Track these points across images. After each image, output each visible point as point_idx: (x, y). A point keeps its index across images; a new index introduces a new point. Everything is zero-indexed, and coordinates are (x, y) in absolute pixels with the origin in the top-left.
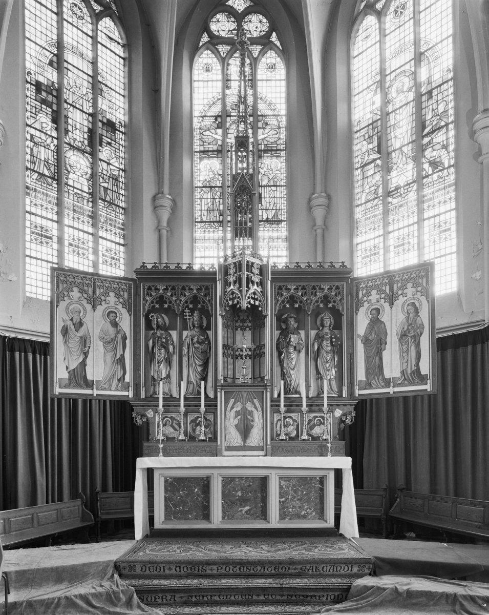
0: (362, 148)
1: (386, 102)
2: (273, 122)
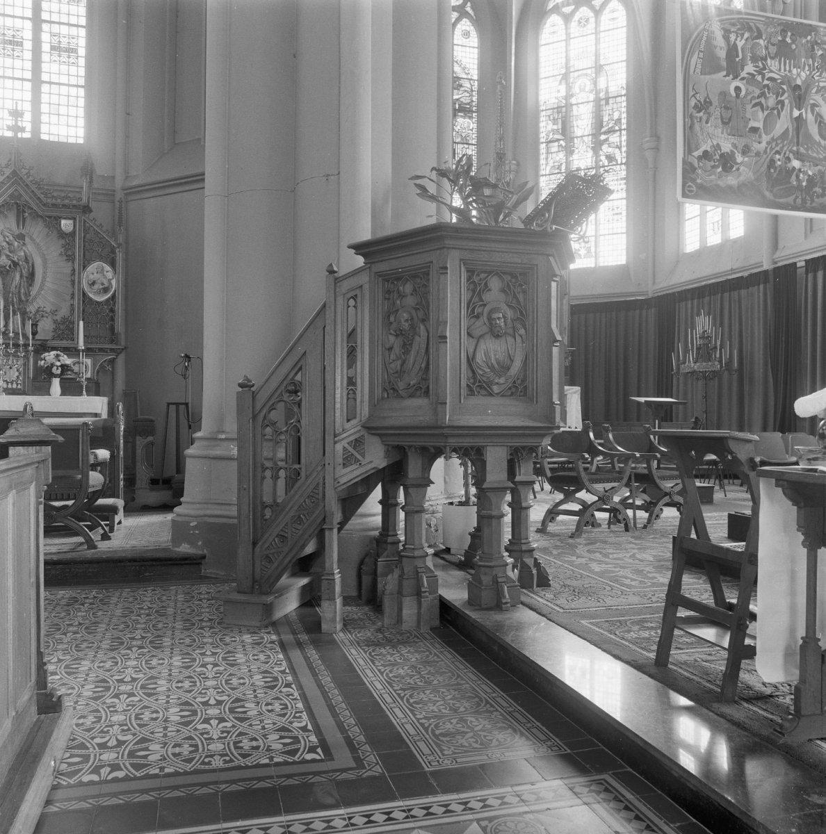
0: (546, 127)
1: (569, 88)
2: (467, 84)
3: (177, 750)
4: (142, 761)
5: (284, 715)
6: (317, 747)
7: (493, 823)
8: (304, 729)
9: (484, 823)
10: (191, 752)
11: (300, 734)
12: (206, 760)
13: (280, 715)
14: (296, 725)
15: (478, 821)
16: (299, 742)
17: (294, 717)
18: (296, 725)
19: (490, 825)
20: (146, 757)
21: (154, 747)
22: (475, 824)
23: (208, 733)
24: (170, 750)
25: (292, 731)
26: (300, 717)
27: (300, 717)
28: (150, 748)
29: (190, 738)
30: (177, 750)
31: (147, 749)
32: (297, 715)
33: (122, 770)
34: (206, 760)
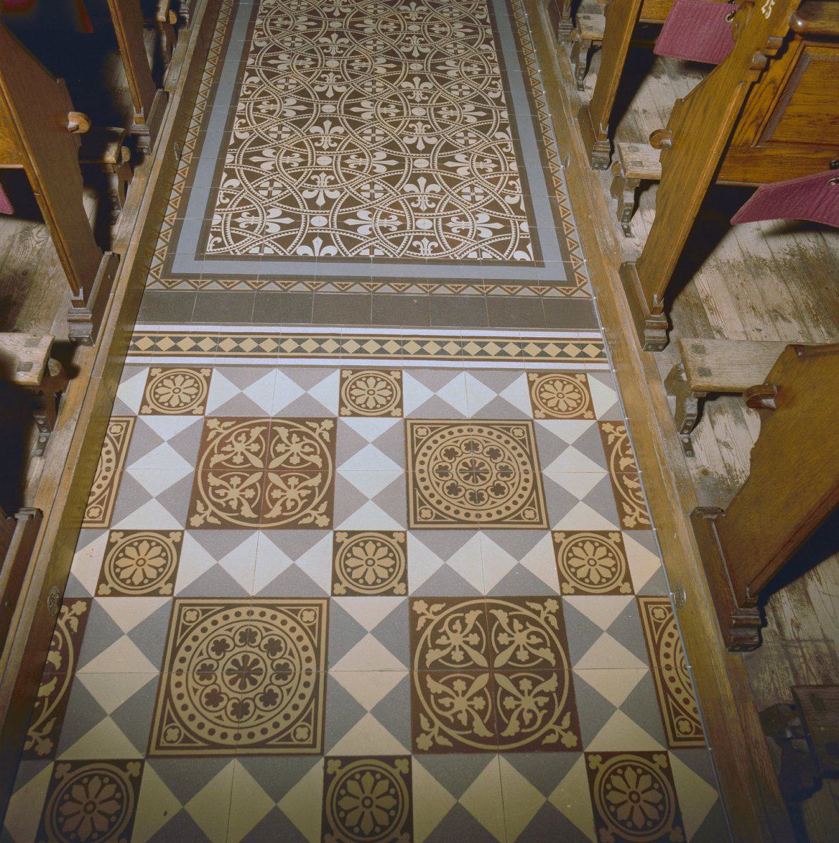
3: (286, 22)
4: (312, 17)
5: (433, 19)
6: (491, 39)
7: (541, 379)
8: (483, 21)
9: (533, 377)
10: (276, 20)
11: (480, 26)
12: (342, 52)
13: (437, 20)
14: (478, 16)
15: (529, 371)
16: (478, 33)
17: (477, 9)
18: (478, 16)
19: (619, 583)
20: (309, 20)
21: (302, 28)
22: (525, 375)
23: (421, 42)
24: (291, 23)
25: (473, 22)
26: (482, 10)
27: (482, 10)
28: (385, 70)
29: (274, 32)
30: (286, 22)
31: (309, 27)
32: (480, 7)
33: (306, 199)
34: (342, 52)
